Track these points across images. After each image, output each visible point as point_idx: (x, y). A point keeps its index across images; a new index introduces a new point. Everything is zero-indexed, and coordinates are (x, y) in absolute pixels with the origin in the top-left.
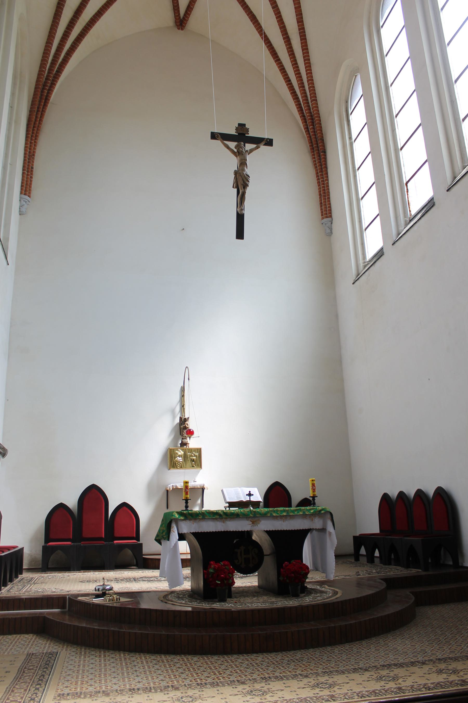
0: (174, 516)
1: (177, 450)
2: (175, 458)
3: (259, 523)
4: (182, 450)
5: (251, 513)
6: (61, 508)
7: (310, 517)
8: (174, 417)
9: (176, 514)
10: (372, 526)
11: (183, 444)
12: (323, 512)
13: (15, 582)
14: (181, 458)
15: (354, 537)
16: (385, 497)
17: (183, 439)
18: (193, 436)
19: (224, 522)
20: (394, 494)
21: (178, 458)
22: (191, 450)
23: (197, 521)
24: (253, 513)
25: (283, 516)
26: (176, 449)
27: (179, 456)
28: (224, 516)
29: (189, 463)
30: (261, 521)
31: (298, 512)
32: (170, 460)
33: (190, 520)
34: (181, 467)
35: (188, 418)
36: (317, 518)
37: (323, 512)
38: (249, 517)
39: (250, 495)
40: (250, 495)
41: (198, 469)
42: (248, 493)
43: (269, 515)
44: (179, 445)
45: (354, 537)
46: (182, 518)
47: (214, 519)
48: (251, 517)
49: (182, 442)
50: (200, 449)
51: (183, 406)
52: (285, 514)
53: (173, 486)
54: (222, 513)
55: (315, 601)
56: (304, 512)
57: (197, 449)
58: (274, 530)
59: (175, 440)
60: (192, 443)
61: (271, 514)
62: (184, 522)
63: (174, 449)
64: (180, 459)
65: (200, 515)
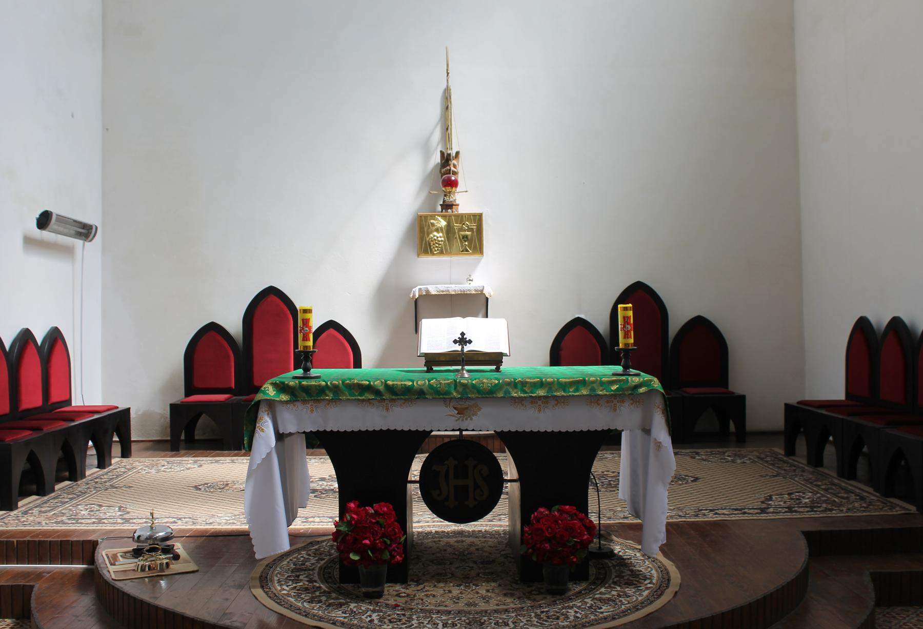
0: (264, 393)
1: (433, 217)
2: (428, 234)
3: (475, 414)
4: (444, 217)
5: (455, 388)
6: (211, 332)
7: (608, 402)
8: (427, 155)
9: (271, 388)
10: (829, 382)
11: (447, 206)
12: (642, 390)
13: (79, 482)
14: (441, 234)
15: (787, 406)
16: (862, 326)
17: (445, 196)
18: (458, 189)
19: (387, 409)
20: (880, 318)
21: (435, 233)
22: (461, 218)
23: (322, 405)
24: (460, 390)
25: (540, 397)
26: (431, 216)
27: (437, 230)
28: (387, 396)
29: (457, 244)
30: (480, 409)
31: (577, 390)
32: (420, 238)
33: (304, 402)
34: (441, 253)
35: (457, 153)
36: (626, 404)
37: (642, 390)
38: (451, 399)
39: (463, 341)
40: (463, 341)
41: (477, 257)
42: (457, 336)
43: (501, 395)
44: (439, 208)
45: (787, 406)
46: (284, 397)
47: (363, 400)
48: (455, 398)
49: (444, 201)
50: (480, 215)
51: (446, 129)
52: (541, 393)
53: (420, 289)
54: (381, 388)
55: (625, 613)
56: (593, 390)
57: (475, 215)
58: (513, 430)
59: (431, 199)
60: (465, 201)
61: (507, 392)
62: (290, 406)
63: (426, 217)
64: (439, 236)
65: (327, 392)
